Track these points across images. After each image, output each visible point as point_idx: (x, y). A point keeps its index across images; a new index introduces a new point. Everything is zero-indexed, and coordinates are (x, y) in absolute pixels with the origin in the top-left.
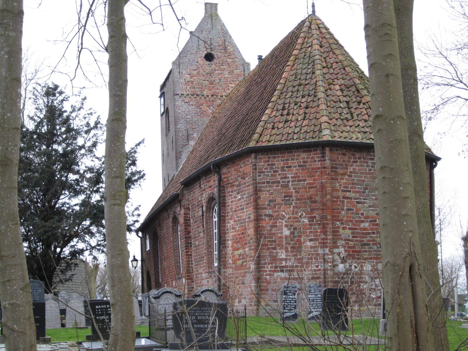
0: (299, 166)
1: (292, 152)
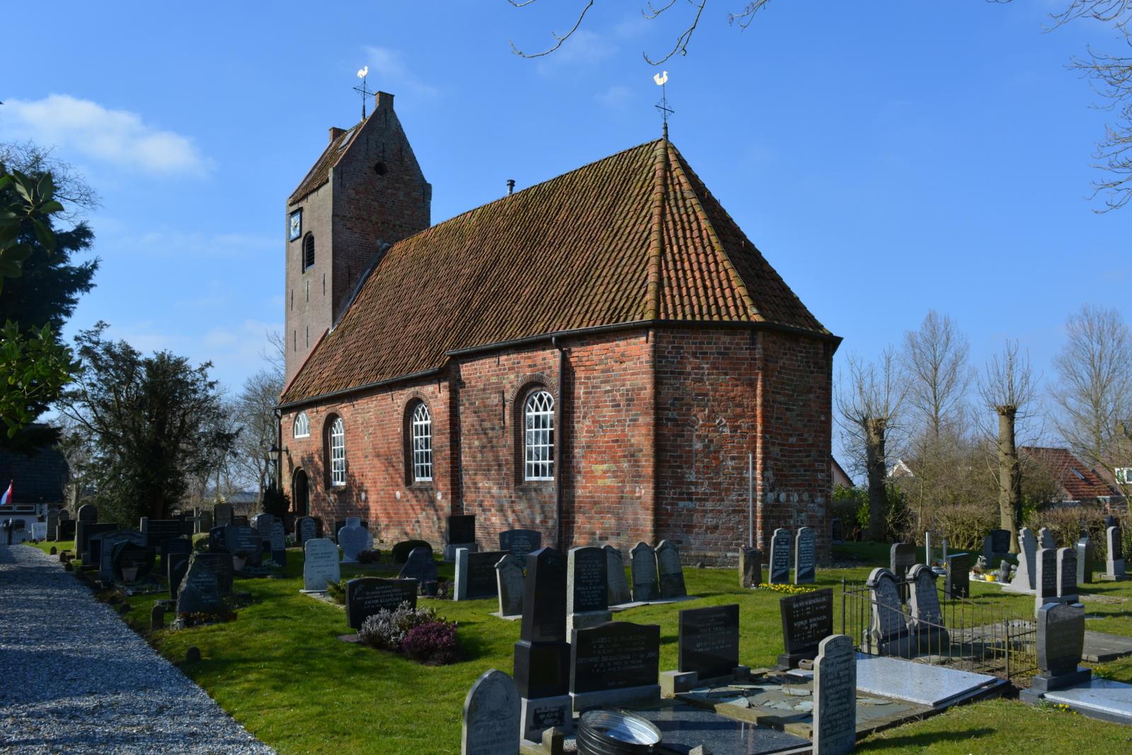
0: (718, 353)
1: (709, 333)
